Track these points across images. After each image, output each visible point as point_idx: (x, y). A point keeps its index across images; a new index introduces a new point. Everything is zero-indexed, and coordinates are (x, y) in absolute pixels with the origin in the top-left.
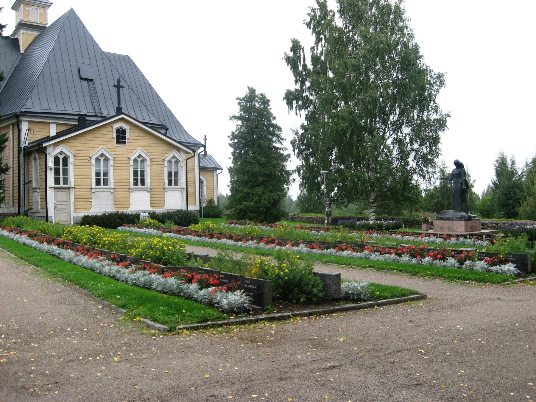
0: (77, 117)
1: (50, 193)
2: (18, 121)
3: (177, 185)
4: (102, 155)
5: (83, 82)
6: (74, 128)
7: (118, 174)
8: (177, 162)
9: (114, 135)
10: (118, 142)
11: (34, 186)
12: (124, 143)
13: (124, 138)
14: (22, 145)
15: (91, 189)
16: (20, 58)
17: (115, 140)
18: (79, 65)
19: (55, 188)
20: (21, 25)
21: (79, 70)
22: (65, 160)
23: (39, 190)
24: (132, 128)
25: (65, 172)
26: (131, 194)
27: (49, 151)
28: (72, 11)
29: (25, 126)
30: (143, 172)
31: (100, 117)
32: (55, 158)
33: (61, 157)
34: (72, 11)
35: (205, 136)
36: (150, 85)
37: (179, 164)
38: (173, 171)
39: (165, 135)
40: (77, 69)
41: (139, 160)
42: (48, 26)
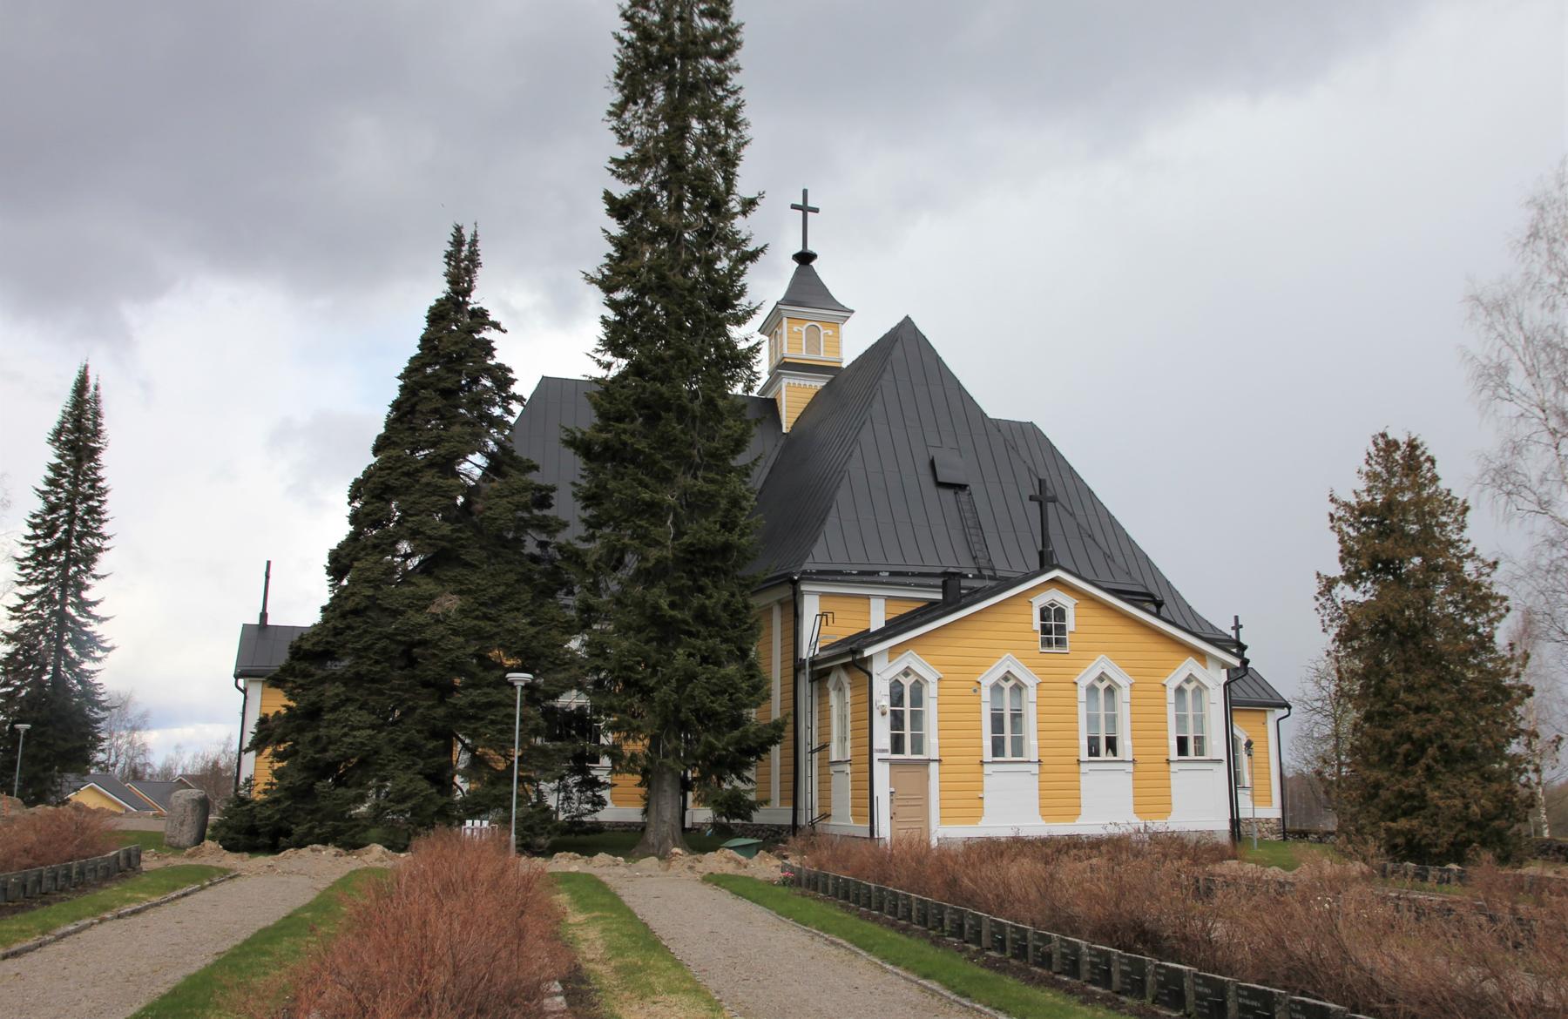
0: (939, 582)
1: (882, 773)
2: (795, 594)
3: (920, 752)
5: (942, 491)
6: (929, 611)
8: (1200, 690)
9: (1037, 623)
10: (1047, 643)
11: (834, 758)
13: (1061, 629)
14: (806, 653)
16: (782, 442)
18: (932, 451)
19: (893, 763)
20: (784, 367)
22: (918, 689)
23: (848, 769)
25: (917, 717)
27: (877, 668)
28: (907, 323)
29: (811, 607)
31: (991, 578)
32: (892, 688)
34: (907, 323)
35: (1236, 618)
36: (1091, 493)
39: (1158, 615)
40: (927, 462)
41: (1189, 688)
42: (844, 365)
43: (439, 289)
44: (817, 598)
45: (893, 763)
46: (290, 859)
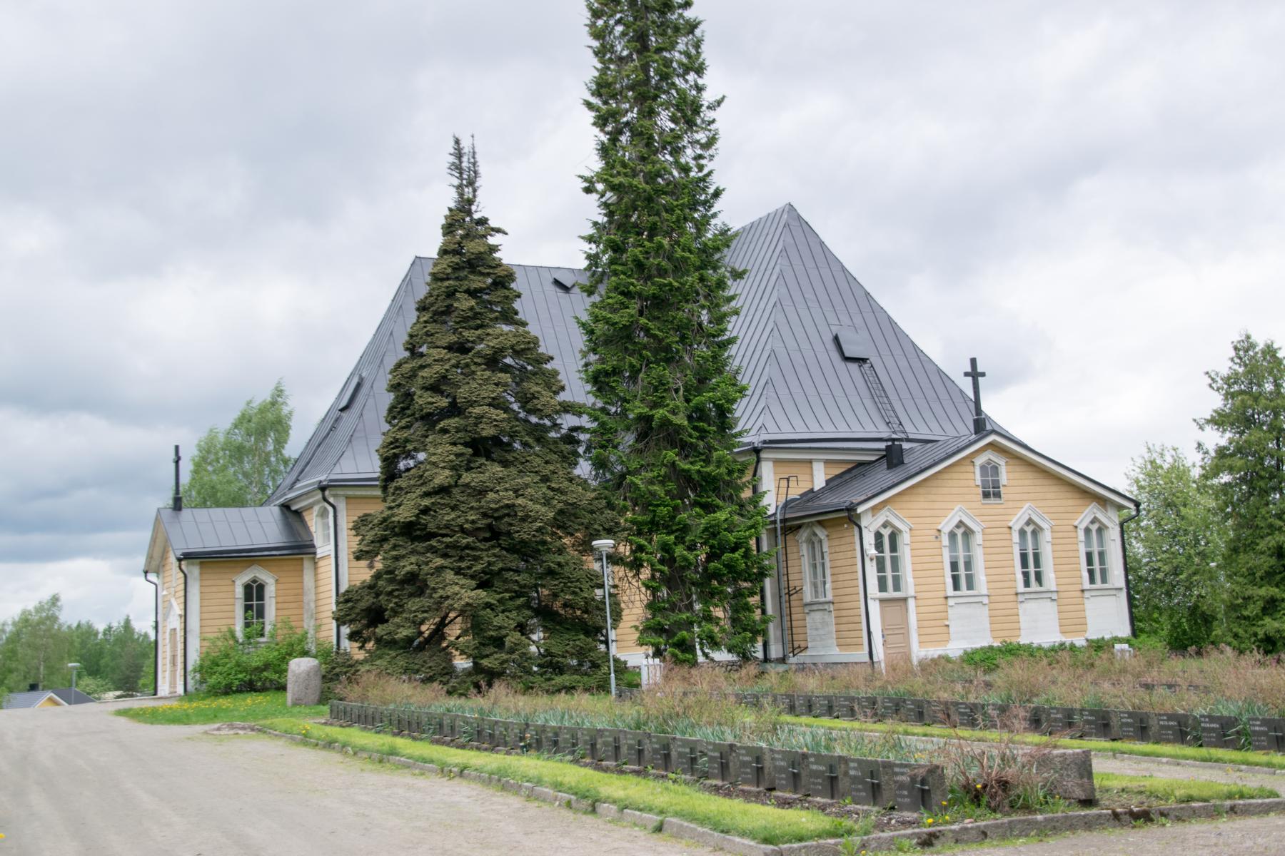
1: (874, 608)
4: (961, 524)
7: (993, 564)
12: (998, 495)
13: (996, 485)
15: (946, 598)
17: (980, 490)
19: (882, 601)
21: (836, 339)
24: (1011, 462)
26: (1022, 608)
27: (864, 522)
28: (1244, 348)
30: (1037, 557)
33: (886, 533)
35: (177, 448)
37: (971, 537)
38: (1095, 550)
40: (828, 339)
43: (449, 199)
44: (770, 464)
45: (882, 601)
46: (381, 736)
